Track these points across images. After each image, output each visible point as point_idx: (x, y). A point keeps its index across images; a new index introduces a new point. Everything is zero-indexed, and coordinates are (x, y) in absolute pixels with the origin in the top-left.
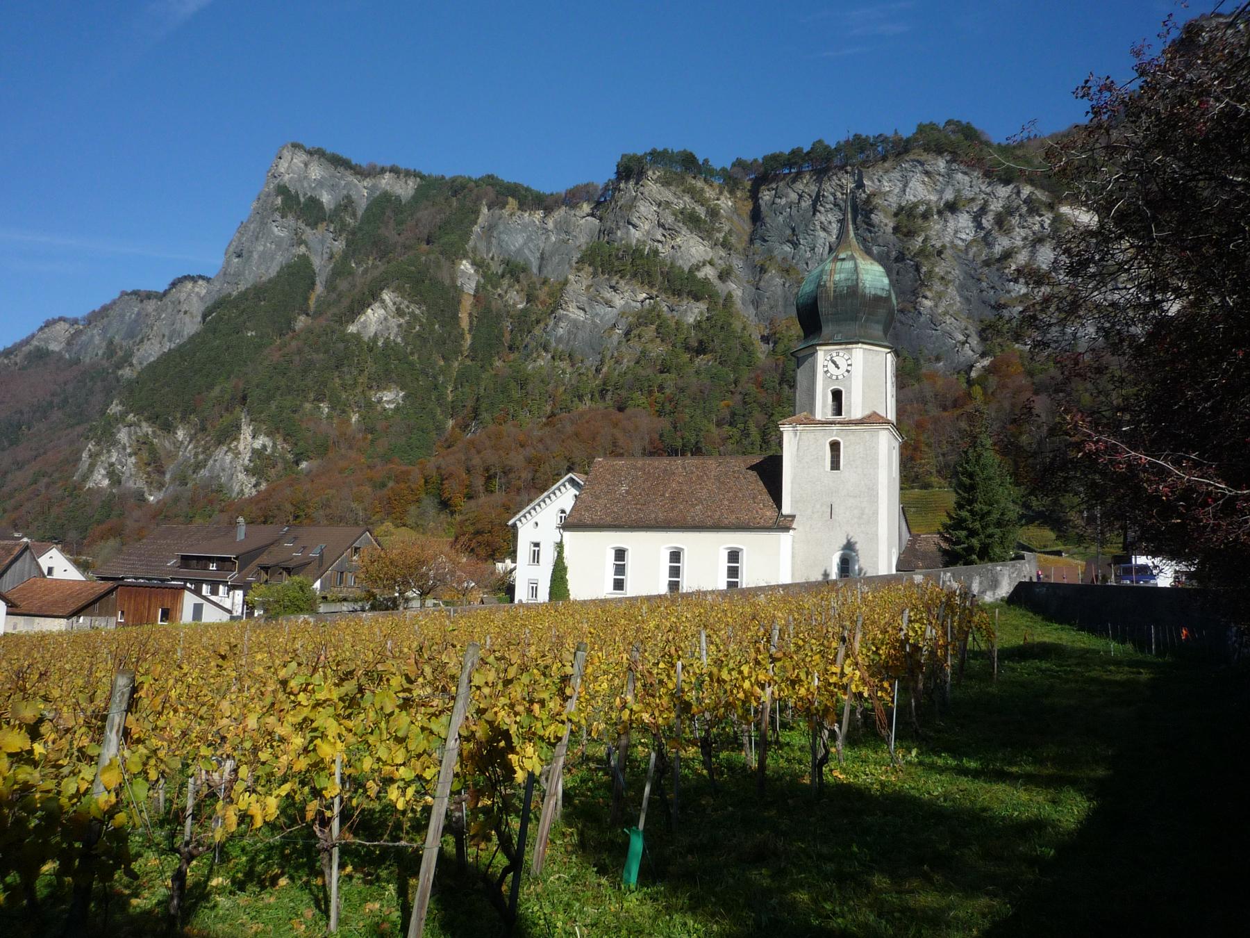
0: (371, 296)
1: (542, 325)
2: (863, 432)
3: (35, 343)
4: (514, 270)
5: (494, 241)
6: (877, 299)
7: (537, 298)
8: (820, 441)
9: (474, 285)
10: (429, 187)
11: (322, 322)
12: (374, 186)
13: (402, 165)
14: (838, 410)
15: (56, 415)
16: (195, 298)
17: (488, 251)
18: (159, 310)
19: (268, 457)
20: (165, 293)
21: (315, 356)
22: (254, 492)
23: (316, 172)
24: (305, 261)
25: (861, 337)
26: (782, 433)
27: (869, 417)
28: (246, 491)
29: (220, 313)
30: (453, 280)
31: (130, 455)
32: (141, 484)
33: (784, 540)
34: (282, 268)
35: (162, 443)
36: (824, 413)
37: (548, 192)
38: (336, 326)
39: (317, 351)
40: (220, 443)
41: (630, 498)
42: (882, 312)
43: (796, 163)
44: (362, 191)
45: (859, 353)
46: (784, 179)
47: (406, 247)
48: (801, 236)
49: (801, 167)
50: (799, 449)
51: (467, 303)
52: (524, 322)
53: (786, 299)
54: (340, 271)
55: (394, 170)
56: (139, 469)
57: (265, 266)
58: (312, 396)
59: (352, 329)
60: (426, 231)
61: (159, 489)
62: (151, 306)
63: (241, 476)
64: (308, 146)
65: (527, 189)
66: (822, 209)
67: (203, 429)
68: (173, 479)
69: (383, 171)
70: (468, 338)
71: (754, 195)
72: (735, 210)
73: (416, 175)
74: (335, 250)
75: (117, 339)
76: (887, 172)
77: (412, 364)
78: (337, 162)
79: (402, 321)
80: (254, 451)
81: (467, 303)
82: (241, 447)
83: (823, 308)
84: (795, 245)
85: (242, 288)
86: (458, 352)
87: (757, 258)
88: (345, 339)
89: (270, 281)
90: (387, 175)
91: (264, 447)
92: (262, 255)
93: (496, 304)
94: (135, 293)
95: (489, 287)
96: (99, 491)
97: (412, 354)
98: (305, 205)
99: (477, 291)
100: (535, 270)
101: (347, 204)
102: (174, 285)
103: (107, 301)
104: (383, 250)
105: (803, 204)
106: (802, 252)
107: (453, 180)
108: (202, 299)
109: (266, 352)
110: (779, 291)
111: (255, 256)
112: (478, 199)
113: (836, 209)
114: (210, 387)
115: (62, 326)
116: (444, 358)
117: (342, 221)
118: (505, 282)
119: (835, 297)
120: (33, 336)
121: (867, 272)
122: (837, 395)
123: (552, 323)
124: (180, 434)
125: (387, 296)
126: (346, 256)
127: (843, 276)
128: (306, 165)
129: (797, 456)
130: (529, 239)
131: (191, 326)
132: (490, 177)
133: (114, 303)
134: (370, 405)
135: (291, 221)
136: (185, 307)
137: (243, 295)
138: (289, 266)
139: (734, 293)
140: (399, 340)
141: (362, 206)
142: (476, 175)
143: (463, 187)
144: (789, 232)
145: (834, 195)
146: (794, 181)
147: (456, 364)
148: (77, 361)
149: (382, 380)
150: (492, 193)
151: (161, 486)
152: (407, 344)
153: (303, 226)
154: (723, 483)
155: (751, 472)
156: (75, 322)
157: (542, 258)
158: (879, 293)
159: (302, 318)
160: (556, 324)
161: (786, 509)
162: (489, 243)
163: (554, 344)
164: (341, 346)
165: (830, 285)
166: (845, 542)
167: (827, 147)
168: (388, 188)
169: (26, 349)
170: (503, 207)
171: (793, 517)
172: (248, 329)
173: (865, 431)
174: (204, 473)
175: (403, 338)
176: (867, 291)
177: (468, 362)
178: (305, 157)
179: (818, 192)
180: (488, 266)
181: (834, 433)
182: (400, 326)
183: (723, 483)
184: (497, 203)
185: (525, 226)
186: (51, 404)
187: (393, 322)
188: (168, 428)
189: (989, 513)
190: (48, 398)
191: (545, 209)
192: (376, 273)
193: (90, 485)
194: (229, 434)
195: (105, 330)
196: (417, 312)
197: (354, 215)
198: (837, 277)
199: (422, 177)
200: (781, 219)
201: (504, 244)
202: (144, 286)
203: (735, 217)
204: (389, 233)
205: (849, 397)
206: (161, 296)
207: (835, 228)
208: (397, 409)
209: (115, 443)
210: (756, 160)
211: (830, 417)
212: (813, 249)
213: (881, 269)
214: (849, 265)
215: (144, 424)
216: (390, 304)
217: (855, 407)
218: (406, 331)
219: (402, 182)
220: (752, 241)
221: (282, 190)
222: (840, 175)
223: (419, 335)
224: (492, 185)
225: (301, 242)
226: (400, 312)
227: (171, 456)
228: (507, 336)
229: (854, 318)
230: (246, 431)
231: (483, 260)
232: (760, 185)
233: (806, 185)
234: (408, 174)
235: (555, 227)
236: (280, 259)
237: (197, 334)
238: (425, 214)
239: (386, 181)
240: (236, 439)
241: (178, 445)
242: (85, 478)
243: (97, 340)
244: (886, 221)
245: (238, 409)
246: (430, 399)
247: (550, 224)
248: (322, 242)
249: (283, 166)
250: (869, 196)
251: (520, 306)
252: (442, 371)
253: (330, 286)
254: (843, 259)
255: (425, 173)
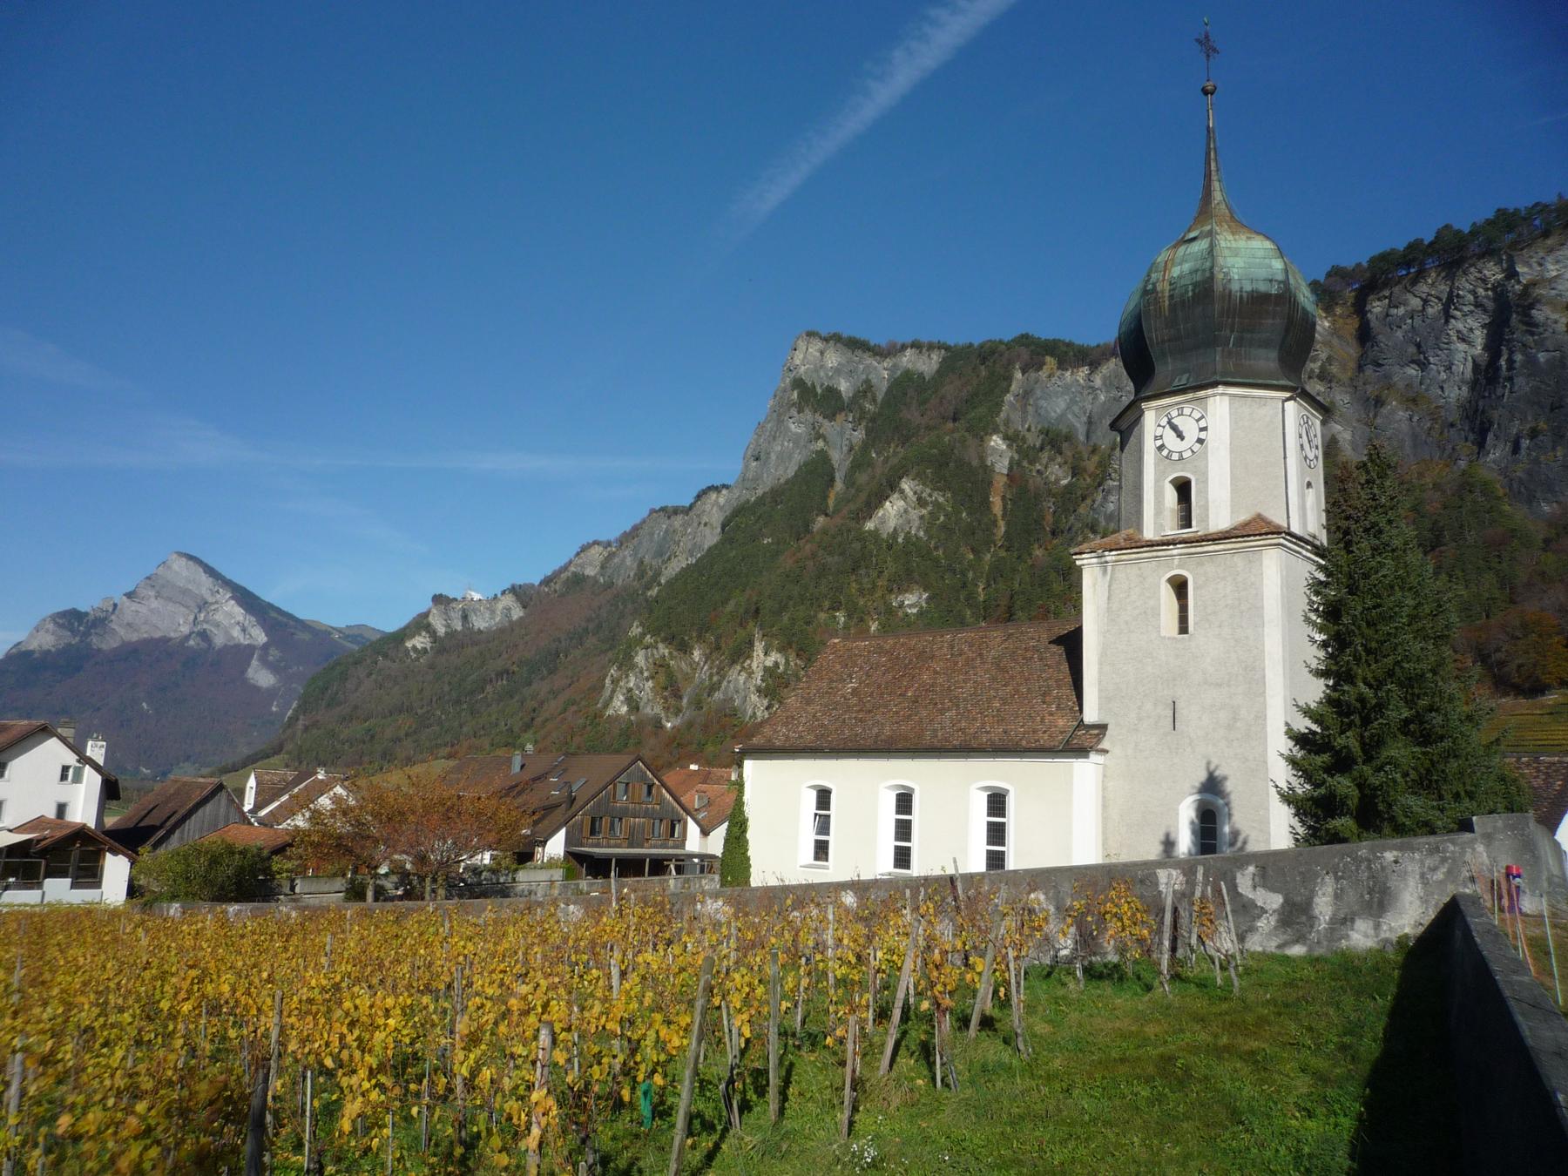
0: (890, 486)
1: (1089, 501)
2: (1229, 558)
3: (572, 569)
4: (1055, 440)
5: (1030, 409)
6: (1258, 301)
7: (1085, 470)
8: (1154, 575)
9: (1006, 463)
10: (956, 358)
11: (838, 520)
12: (895, 365)
13: (924, 339)
14: (1186, 521)
15: (590, 642)
16: (715, 511)
17: (1024, 420)
18: (685, 525)
19: (781, 676)
20: (691, 507)
21: (829, 559)
22: (766, 715)
23: (833, 359)
24: (823, 457)
25: (1224, 374)
26: (1079, 570)
27: (1246, 524)
28: (759, 714)
29: (739, 522)
30: (982, 459)
31: (647, 679)
32: (658, 710)
33: (1084, 772)
34: (800, 468)
35: (678, 664)
36: (1159, 526)
37: (1093, 344)
38: (853, 524)
39: (831, 554)
40: (733, 662)
41: (854, 700)
42: (1272, 325)
43: (1414, 260)
44: (881, 373)
45: (1220, 406)
46: (1399, 282)
47: (929, 428)
48: (1430, 353)
49: (1422, 263)
50: (1113, 600)
51: (1000, 482)
52: (1069, 499)
53: (1415, 437)
54: (859, 462)
55: (916, 345)
56: (656, 694)
57: (783, 468)
58: (827, 604)
59: (870, 525)
60: (951, 408)
61: (676, 715)
62: (678, 521)
63: (754, 698)
64: (824, 334)
65: (1069, 345)
66: (1458, 313)
67: (718, 648)
68: (689, 703)
69: (904, 347)
70: (1002, 524)
71: (1360, 308)
72: (1334, 331)
73: (940, 346)
74: (854, 441)
75: (647, 560)
76: (1551, 250)
77: (936, 561)
78: (854, 344)
79: (924, 511)
80: (766, 669)
81: (1000, 482)
82: (754, 666)
83: (1155, 333)
84: (1423, 365)
85: (760, 492)
86: (989, 542)
87: (1369, 389)
88: (862, 537)
89: (787, 482)
90: (908, 352)
91: (776, 664)
92: (780, 456)
93: (1035, 482)
94: (663, 509)
95: (1025, 464)
96: (617, 718)
97: (936, 548)
98: (823, 395)
99: (1010, 468)
100: (1082, 438)
101: (866, 390)
102: (699, 497)
103: (638, 521)
104: (905, 434)
105: (1430, 310)
106: (1433, 373)
107: (981, 346)
108: (721, 508)
109: (781, 558)
110: (1405, 426)
111: (773, 457)
112: (1010, 363)
113: (1479, 311)
114: (725, 602)
115: (597, 549)
116: (973, 550)
117: (862, 409)
118: (1045, 456)
119: (1173, 307)
120: (571, 562)
121: (1236, 253)
122: (1183, 489)
123: (1099, 498)
124: (697, 654)
125: (906, 485)
126: (865, 447)
127: (1186, 267)
128: (822, 353)
129: (1109, 609)
130: (1073, 401)
131: (711, 537)
132: (1025, 337)
133: (644, 521)
134: (890, 611)
135: (808, 415)
136: (705, 519)
137: (761, 501)
138: (806, 464)
139: (1339, 437)
140: (922, 534)
141: (882, 388)
142: (1008, 336)
143: (993, 352)
144: (1412, 349)
145: (1474, 293)
146: (1414, 282)
147: (989, 556)
148: (610, 585)
149: (902, 582)
150: (1025, 354)
151: (678, 711)
152: (931, 537)
153: (820, 419)
154: (1004, 670)
155: (1054, 648)
156: (609, 544)
157: (1090, 422)
158: (1263, 287)
159: (821, 519)
160: (1105, 499)
161: (1091, 715)
162: (1024, 412)
163: (1103, 524)
164: (857, 545)
165: (1164, 288)
166: (1202, 776)
167: (1459, 231)
168: (910, 366)
169: (564, 576)
170: (1040, 368)
171: (1103, 728)
172: (764, 536)
173: (1237, 551)
174: (718, 695)
175: (926, 532)
176: (1235, 287)
177: (1002, 553)
178: (820, 345)
179: (1451, 292)
180: (1024, 439)
181: (1176, 562)
182: (922, 517)
183: (1004, 670)
184: (1033, 365)
185: (1067, 388)
186: (586, 630)
187: (914, 514)
188: (685, 649)
189: (1380, 707)
190: (584, 624)
191: (1091, 364)
192: (895, 461)
193: (610, 712)
194: (741, 653)
195: (635, 550)
196: (941, 499)
197: (874, 400)
198: (1176, 271)
199: (947, 348)
200: (1399, 334)
201: (1042, 412)
202: (672, 502)
203: (1335, 341)
204: (912, 415)
205: (1204, 492)
206: (687, 511)
207: (1479, 337)
208: (921, 613)
209: (633, 666)
210: (1359, 265)
211: (1171, 530)
212: (1449, 368)
213: (1268, 245)
214: (1201, 246)
215: (661, 646)
216: (909, 493)
217: (1217, 511)
218: (929, 523)
219: (925, 357)
220: (1360, 368)
221: (798, 383)
222: (1480, 265)
223: (944, 527)
224: (1027, 346)
225: (819, 436)
226: (921, 502)
227: (688, 678)
228: (1050, 518)
229: (1211, 342)
230: (759, 647)
231: (1017, 433)
232: (1367, 295)
233: (1433, 286)
234: (931, 347)
235: (1104, 384)
236: (798, 458)
237: (716, 546)
238: (950, 390)
239: (908, 359)
240: (750, 657)
241: (694, 666)
242: (606, 706)
243: (629, 561)
244: (1555, 316)
245: (751, 624)
246: (958, 600)
247: (1098, 381)
248: (842, 434)
249: (798, 358)
250: (1526, 287)
251: (1064, 482)
252: (971, 566)
253: (850, 481)
254: (1194, 239)
255: (951, 342)
